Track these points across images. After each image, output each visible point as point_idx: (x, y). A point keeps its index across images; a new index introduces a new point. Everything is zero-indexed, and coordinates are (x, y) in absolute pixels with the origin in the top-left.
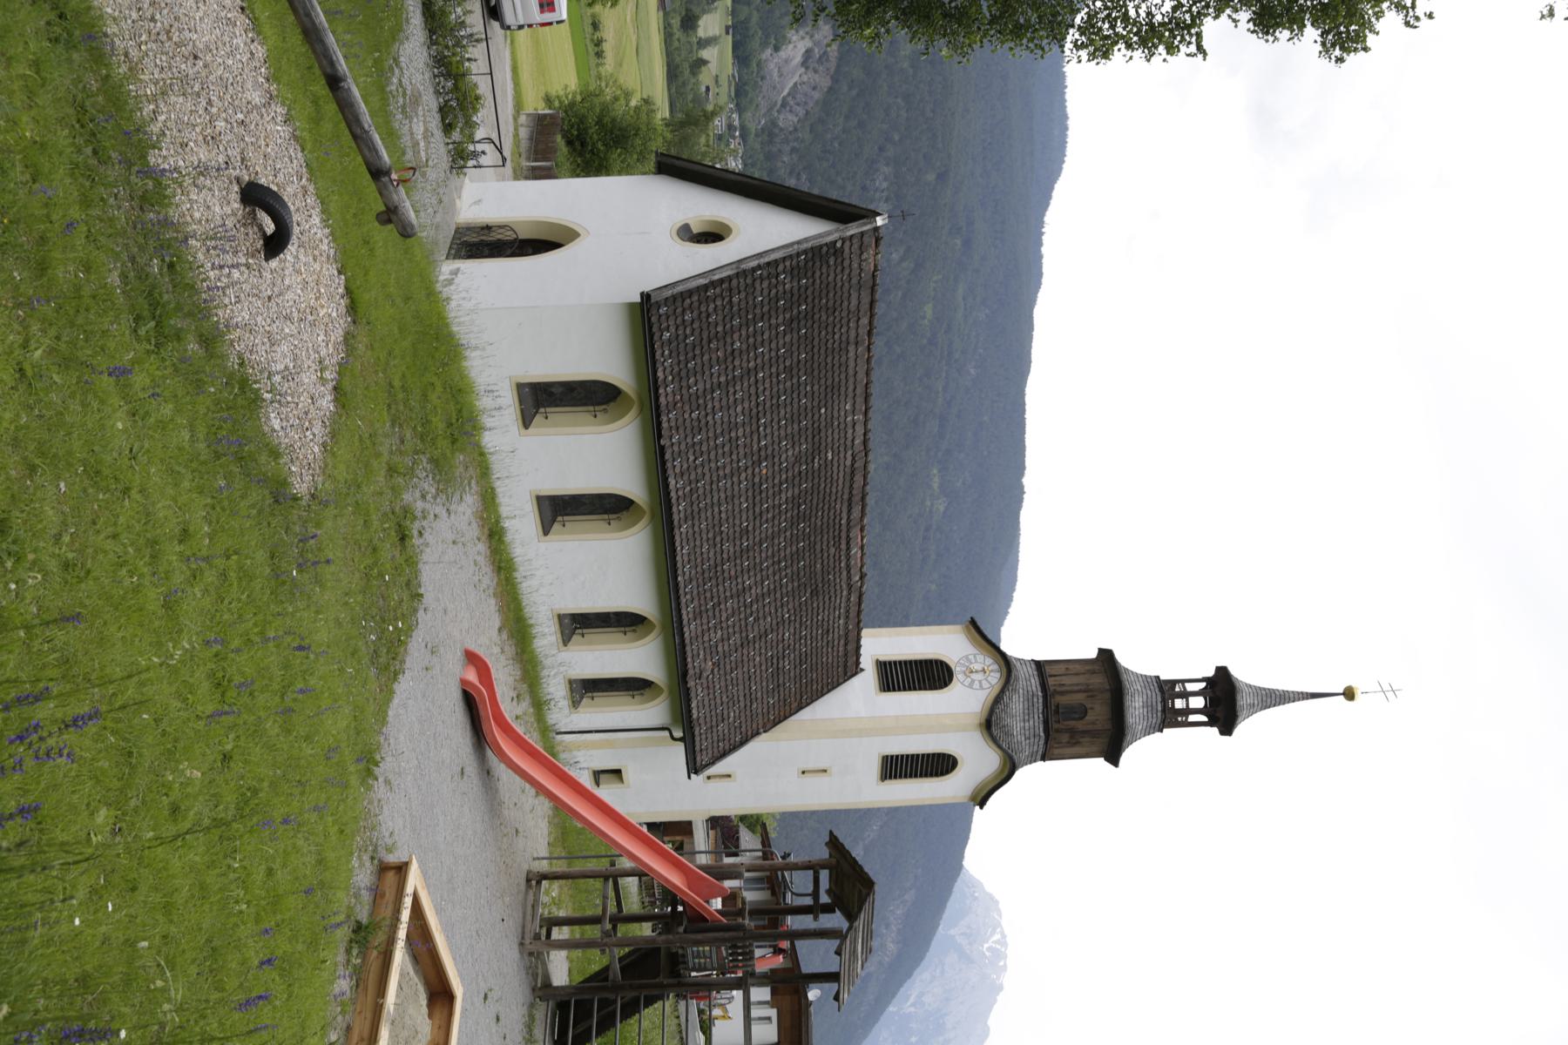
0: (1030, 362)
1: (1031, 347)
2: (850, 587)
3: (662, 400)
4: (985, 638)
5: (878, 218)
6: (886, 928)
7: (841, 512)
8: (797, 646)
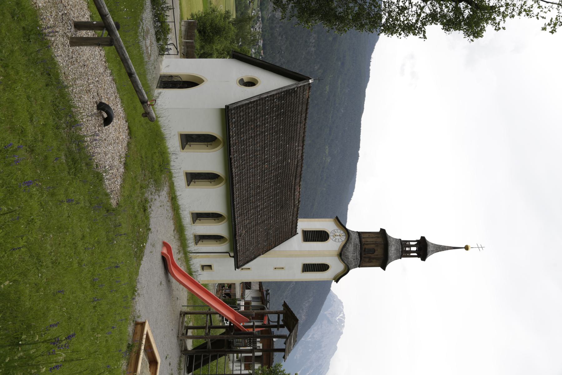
1: (364, 103)
2: (294, 205)
3: (231, 142)
4: (341, 223)
5: (310, 80)
6: (302, 311)
8: (275, 225)
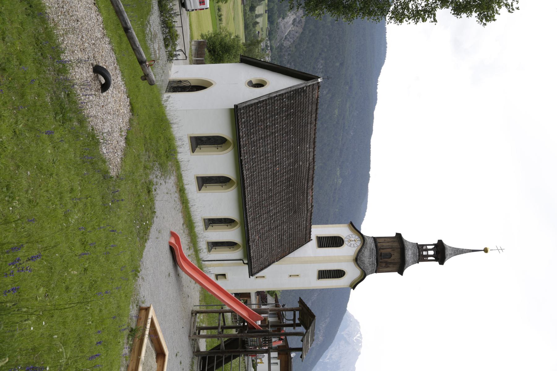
0: (373, 130)
2: (308, 210)
3: (241, 143)
5: (319, 79)
6: (319, 332)
8: (289, 231)
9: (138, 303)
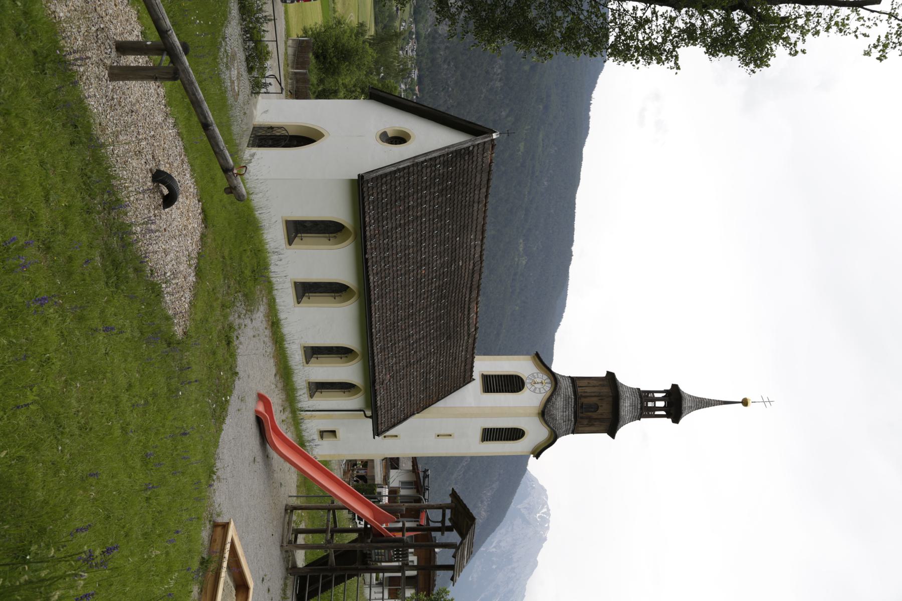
0: (580, 179)
2: (469, 335)
3: (368, 233)
4: (543, 363)
5: (494, 134)
6: (481, 504)
7: (466, 294)
8: (438, 366)
9: (211, 517)
